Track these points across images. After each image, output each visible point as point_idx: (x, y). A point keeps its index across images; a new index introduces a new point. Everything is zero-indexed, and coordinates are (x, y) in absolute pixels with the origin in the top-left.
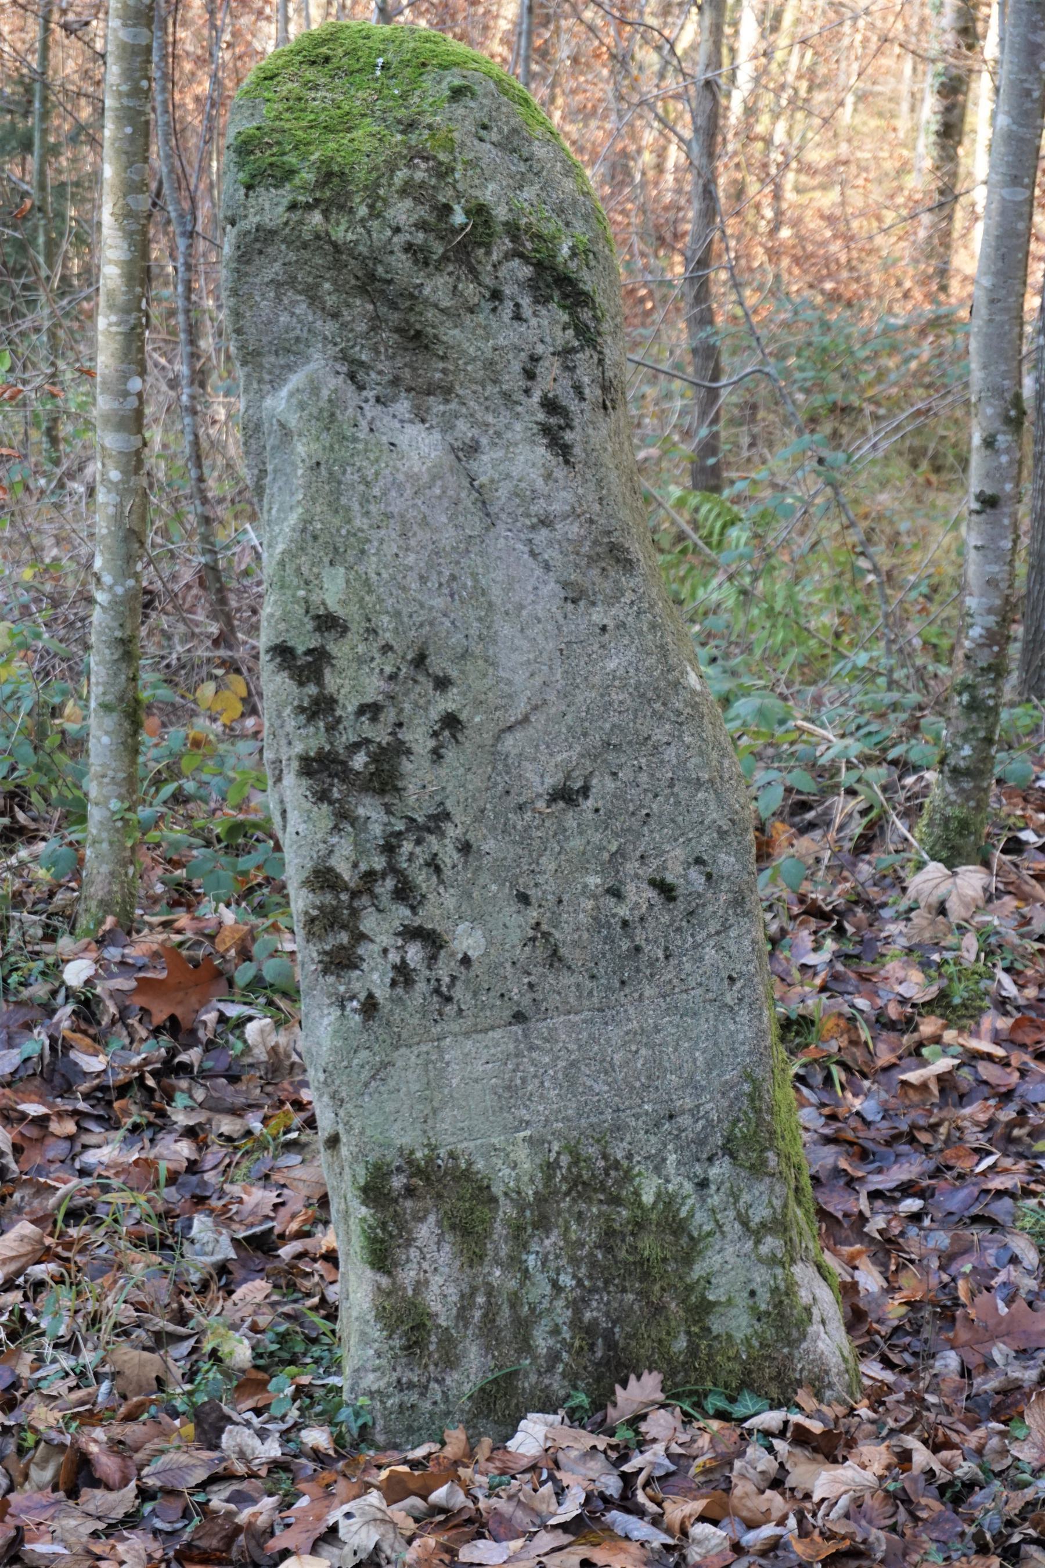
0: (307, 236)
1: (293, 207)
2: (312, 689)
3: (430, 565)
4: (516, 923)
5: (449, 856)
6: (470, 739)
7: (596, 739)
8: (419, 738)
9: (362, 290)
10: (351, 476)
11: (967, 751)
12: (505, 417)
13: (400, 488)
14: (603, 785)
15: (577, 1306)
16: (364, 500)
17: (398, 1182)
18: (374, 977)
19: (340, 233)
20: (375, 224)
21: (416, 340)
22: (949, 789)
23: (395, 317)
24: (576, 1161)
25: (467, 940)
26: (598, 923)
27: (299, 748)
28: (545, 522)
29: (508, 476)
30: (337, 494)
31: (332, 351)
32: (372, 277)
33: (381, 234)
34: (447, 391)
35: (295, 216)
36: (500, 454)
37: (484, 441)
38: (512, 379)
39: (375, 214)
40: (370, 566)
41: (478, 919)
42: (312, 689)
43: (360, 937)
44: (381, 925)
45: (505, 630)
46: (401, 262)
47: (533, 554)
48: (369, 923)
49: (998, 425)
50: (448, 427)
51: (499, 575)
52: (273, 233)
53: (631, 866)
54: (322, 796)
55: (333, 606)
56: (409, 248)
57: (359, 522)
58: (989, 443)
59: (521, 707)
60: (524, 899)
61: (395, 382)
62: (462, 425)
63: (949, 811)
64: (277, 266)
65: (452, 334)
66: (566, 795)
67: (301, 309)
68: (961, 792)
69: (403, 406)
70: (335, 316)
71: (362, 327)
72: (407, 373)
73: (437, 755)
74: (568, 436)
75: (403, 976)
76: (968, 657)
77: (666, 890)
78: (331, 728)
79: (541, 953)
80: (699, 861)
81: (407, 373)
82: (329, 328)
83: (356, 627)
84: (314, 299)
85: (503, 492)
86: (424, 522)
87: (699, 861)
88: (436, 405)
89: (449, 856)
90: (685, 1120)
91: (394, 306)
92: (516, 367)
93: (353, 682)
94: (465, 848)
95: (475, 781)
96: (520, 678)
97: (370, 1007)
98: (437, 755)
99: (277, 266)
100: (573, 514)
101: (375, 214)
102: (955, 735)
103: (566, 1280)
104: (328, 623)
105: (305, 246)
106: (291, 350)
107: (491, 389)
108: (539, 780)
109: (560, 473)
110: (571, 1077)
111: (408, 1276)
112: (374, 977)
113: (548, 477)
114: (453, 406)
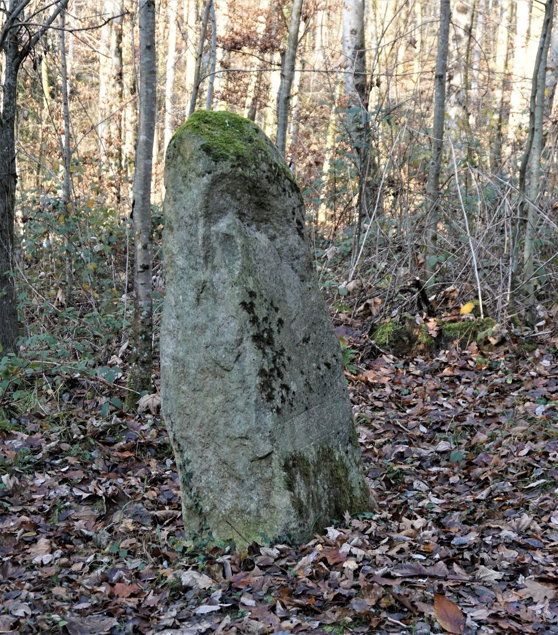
0: (237, 175)
1: (233, 166)
2: (252, 315)
3: (271, 274)
4: (301, 379)
5: (286, 362)
6: (286, 325)
7: (310, 322)
8: (275, 327)
9: (249, 192)
10: (251, 249)
11: (146, 355)
12: (286, 227)
13: (261, 250)
14: (313, 336)
15: (329, 494)
16: (255, 256)
17: (291, 463)
18: (278, 402)
19: (248, 174)
20: (258, 170)
21: (261, 206)
22: (141, 369)
23: (256, 199)
24: (323, 450)
25: (293, 387)
26: (317, 378)
27: (252, 333)
28: (297, 258)
29: (287, 245)
30: (248, 254)
31: (235, 211)
32: (254, 187)
33: (260, 174)
34: (266, 221)
35: (234, 169)
36: (283, 238)
37: (278, 235)
38: (290, 215)
39: (257, 167)
40: (258, 276)
41: (294, 380)
42: (252, 315)
43: (273, 389)
44: (276, 385)
45: (288, 292)
46: (265, 181)
47: (293, 268)
48: (274, 385)
49: (148, 241)
50: (266, 232)
51: (285, 275)
52: (226, 175)
53: (320, 359)
54: (259, 347)
55: (252, 289)
56: (267, 177)
57: (254, 262)
58: (145, 247)
59: (294, 314)
60: (302, 373)
61: (253, 219)
62: (271, 231)
63: (142, 376)
64: (224, 185)
65: (275, 203)
66: (306, 340)
67: (229, 198)
68: (145, 369)
69: (254, 227)
70: (239, 200)
71: (246, 203)
72: (256, 216)
73: (279, 331)
74: (303, 231)
75: (283, 400)
76: (142, 322)
77: (328, 365)
78: (258, 326)
79: (308, 388)
80: (334, 356)
81: (256, 216)
82: (236, 204)
83: (258, 294)
84: (233, 194)
85: (285, 250)
86: (268, 261)
87: (334, 356)
88: (263, 225)
89: (286, 362)
90: (341, 434)
91: (257, 195)
92: (291, 211)
93: (261, 312)
94: (289, 359)
95: (288, 339)
96: (293, 306)
97: (279, 411)
98: (279, 331)
99: (224, 185)
100: (304, 254)
101: (257, 167)
102: (141, 350)
103: (326, 486)
104: (252, 294)
105: (235, 178)
106: (222, 212)
107: (284, 219)
108: (300, 337)
109: (302, 242)
110: (318, 426)
111: (297, 491)
112: (278, 402)
113: (299, 244)
114: (269, 225)
